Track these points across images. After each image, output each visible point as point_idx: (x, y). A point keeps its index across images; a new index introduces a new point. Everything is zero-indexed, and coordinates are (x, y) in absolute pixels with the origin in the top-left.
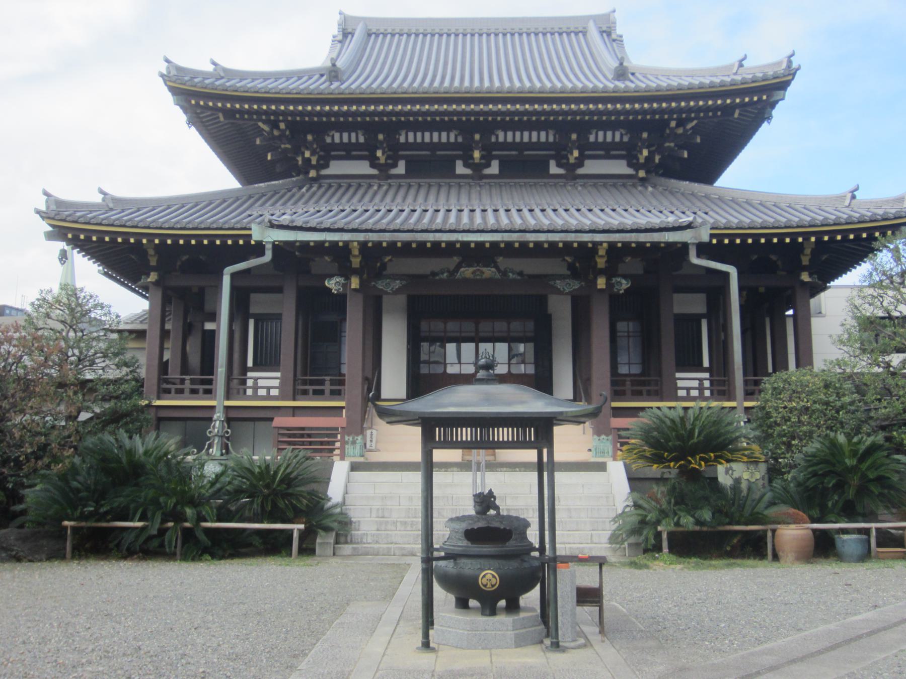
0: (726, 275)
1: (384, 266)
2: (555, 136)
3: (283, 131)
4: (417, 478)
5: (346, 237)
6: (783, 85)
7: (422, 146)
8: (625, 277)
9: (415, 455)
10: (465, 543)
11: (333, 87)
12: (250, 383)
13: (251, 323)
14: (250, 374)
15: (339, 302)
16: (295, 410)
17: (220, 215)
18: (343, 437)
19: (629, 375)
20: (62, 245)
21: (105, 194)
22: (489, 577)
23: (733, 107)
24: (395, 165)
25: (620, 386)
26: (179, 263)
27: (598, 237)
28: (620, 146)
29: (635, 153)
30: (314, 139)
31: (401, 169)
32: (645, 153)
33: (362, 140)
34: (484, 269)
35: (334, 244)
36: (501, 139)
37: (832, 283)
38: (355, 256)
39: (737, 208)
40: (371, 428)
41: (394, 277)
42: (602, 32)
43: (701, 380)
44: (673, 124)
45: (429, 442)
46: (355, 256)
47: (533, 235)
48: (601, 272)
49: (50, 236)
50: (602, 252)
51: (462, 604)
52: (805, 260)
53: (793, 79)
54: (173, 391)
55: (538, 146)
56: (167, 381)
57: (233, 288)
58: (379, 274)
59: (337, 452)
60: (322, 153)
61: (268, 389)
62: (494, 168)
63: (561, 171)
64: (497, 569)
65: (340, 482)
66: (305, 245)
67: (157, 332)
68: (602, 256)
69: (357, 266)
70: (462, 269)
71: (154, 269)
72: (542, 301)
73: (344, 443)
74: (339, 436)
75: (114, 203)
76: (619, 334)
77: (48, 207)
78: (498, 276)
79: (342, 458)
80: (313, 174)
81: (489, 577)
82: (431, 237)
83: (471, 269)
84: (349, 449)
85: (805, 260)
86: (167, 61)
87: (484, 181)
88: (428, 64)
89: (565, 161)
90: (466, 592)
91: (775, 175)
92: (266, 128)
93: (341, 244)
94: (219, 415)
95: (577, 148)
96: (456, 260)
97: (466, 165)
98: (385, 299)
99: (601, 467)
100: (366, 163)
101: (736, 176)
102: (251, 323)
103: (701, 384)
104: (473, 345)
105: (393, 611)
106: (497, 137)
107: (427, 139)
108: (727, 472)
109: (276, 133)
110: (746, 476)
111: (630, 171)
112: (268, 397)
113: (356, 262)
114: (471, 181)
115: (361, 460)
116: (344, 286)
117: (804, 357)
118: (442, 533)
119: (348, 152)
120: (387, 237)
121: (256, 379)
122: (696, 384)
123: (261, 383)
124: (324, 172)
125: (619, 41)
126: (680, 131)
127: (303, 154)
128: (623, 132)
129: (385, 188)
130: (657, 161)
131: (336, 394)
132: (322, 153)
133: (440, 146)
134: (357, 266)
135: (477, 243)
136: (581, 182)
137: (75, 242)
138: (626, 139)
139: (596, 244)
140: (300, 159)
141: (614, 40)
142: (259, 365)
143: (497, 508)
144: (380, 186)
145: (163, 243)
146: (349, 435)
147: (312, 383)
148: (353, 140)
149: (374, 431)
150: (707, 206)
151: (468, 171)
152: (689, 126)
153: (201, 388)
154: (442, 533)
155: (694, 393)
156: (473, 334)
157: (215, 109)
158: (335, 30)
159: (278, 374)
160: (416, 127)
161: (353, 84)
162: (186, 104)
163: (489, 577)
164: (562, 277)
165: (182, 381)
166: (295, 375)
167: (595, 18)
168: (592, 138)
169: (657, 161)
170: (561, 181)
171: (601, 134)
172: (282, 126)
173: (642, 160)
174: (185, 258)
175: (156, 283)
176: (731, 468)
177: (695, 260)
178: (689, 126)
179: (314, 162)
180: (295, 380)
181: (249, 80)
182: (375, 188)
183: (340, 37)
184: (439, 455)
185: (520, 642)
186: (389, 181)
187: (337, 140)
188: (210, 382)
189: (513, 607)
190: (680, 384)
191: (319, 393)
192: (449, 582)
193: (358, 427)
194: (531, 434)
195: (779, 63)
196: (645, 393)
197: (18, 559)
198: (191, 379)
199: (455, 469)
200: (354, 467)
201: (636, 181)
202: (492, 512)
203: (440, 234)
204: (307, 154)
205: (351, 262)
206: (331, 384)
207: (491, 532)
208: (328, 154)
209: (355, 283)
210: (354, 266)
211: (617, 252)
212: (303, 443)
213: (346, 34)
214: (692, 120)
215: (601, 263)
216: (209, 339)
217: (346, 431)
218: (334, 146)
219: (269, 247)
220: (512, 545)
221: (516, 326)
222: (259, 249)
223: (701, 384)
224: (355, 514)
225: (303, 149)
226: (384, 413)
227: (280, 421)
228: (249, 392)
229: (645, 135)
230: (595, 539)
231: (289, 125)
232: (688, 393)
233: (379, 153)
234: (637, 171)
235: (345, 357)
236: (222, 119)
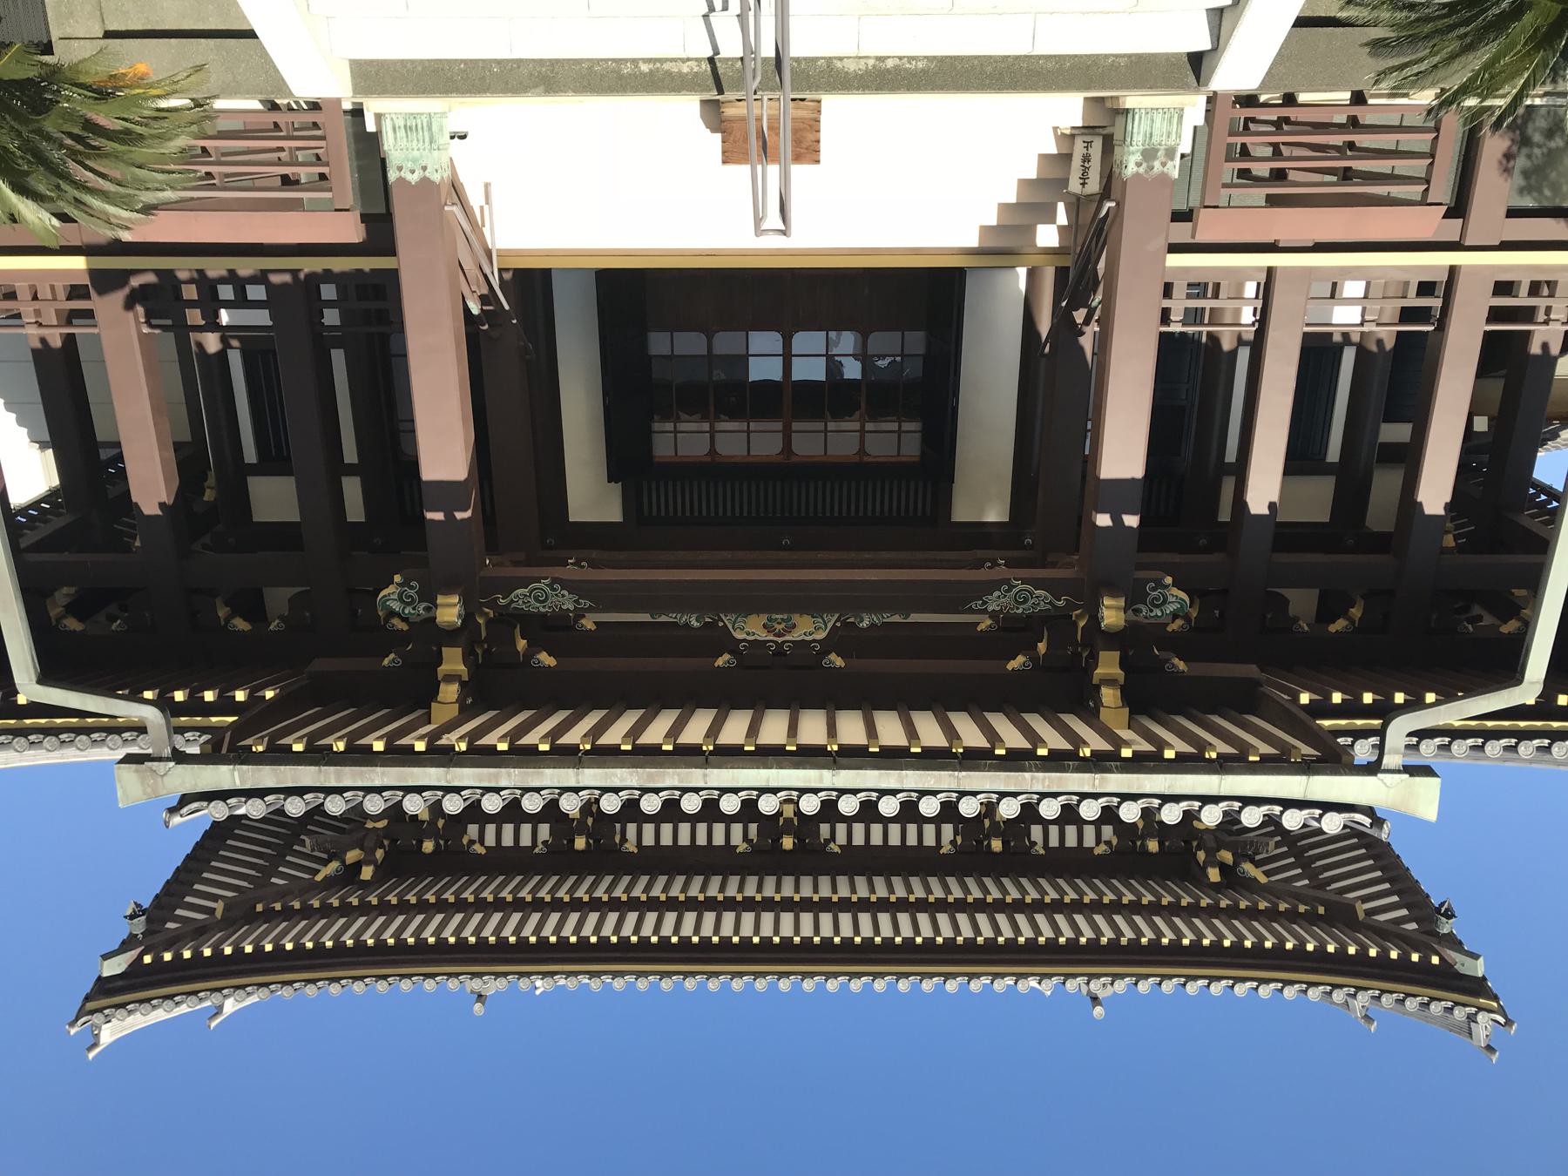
2: (624, 839)
3: (1212, 861)
13: (1334, 453)
34: (763, 635)
38: (1110, 682)
46: (1110, 682)
48: (450, 636)
50: (449, 692)
53: (87, 999)
68: (450, 678)
69: (1104, 656)
70: (821, 635)
78: (727, 620)
83: (796, 636)
91: (129, 789)
102: (1334, 453)
109: (1227, 856)
113: (1108, 665)
126: (352, 856)
128: (478, 849)
134: (1104, 656)
146: (1164, 177)
153: (1522, 300)
171: (526, 841)
172: (1214, 875)
199: (851, 66)
210: (1115, 655)
229: (428, 846)
231: (1200, 881)
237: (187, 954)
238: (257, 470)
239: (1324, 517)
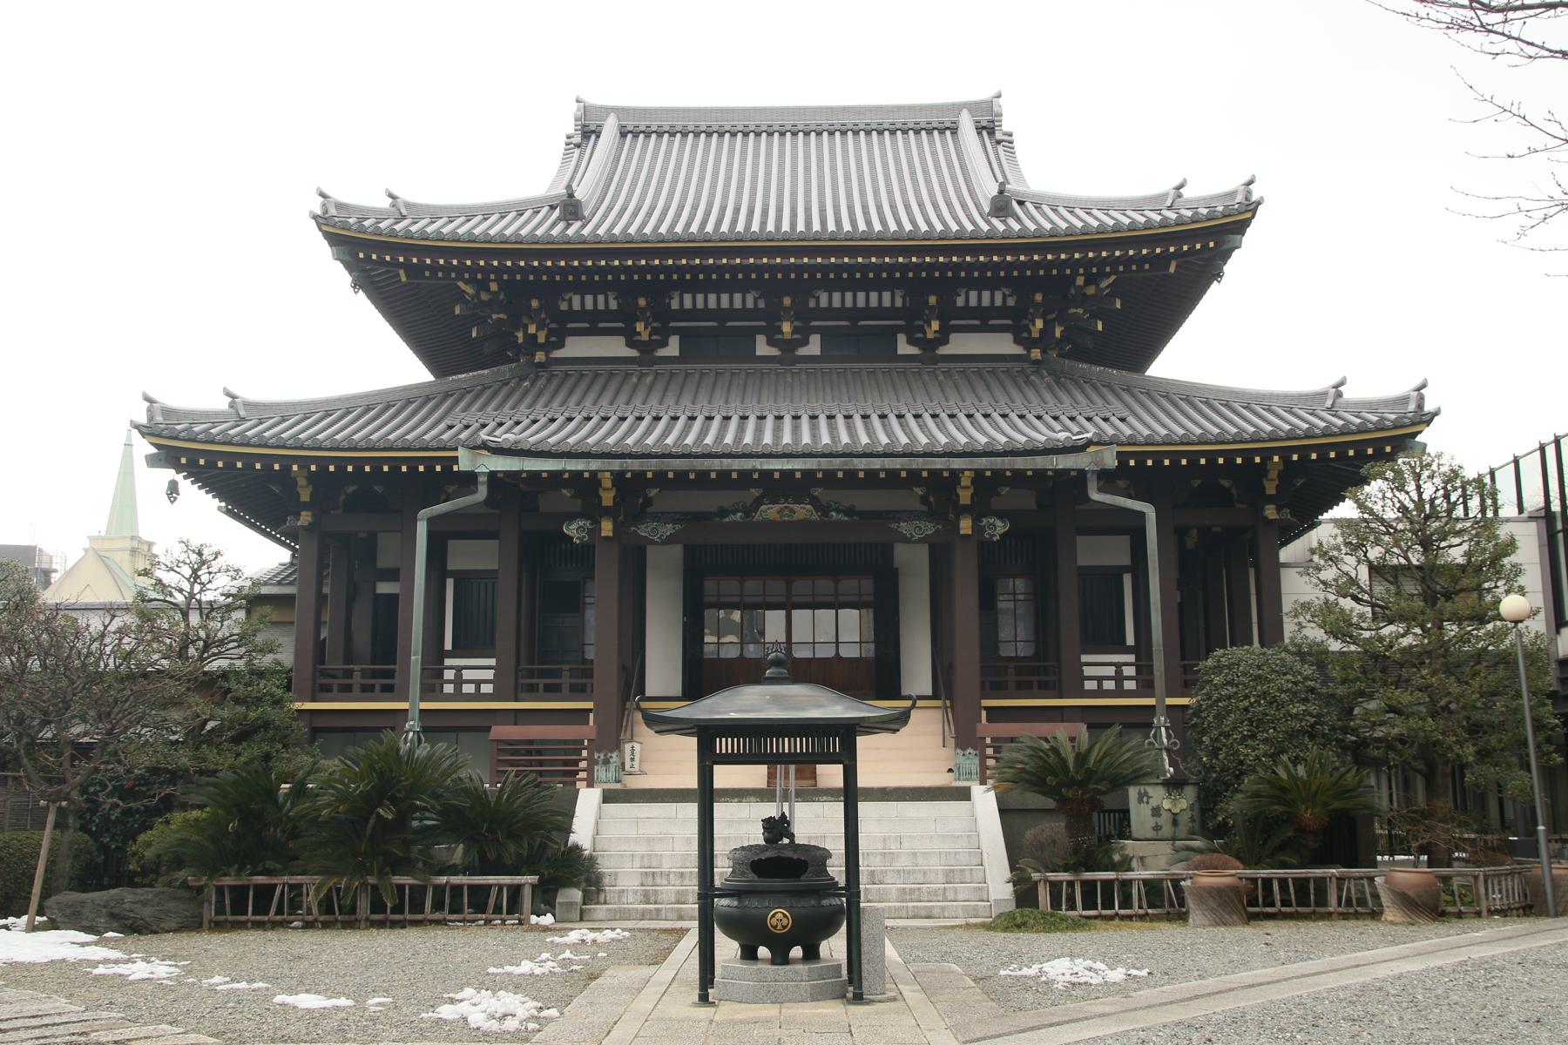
0: (1142, 515)
1: (649, 502)
4: (691, 810)
5: (594, 465)
6: (1240, 227)
7: (706, 314)
8: (1001, 515)
9: (691, 781)
10: (753, 876)
11: (570, 232)
12: (449, 675)
13: (450, 583)
14: (448, 662)
15: (585, 555)
16: (517, 716)
17: (409, 425)
18: (591, 754)
19: (1017, 659)
20: (169, 474)
21: (234, 397)
22: (779, 918)
23: (1166, 258)
25: (999, 675)
26: (343, 497)
27: (957, 463)
28: (1003, 312)
29: (1025, 322)
30: (541, 306)
31: (673, 348)
32: (1039, 324)
33: (613, 305)
34: (796, 507)
35: (577, 475)
36: (824, 303)
37: (1326, 516)
39: (1171, 409)
40: (631, 740)
41: (663, 517)
42: (980, 130)
43: (1118, 666)
44: (1080, 281)
45: (708, 759)
48: (966, 510)
49: (153, 461)
51: (749, 954)
52: (1271, 489)
54: (335, 688)
55: (880, 313)
56: (324, 674)
57: (431, 535)
58: (640, 516)
59: (582, 775)
60: (553, 326)
61: (478, 683)
62: (814, 347)
63: (913, 350)
64: (787, 908)
65: (589, 819)
66: (535, 475)
67: (312, 600)
71: (306, 506)
72: (887, 551)
73: (592, 763)
74: (585, 753)
75: (240, 409)
77: (151, 418)
78: (815, 517)
79: (590, 785)
80: (540, 357)
81: (779, 918)
82: (716, 464)
83: (777, 507)
84: (600, 771)
85: (1271, 489)
86: (322, 195)
87: (798, 366)
88: (712, 195)
89: (920, 335)
90: (751, 935)
91: (1233, 351)
92: (469, 289)
93: (586, 475)
94: (413, 724)
95: (938, 318)
96: (755, 492)
97: (771, 343)
98: (650, 549)
99: (964, 795)
100: (621, 340)
101: (1174, 362)
102: (450, 583)
103: (1119, 672)
104: (782, 613)
105: (665, 972)
106: (818, 299)
107: (712, 304)
108: (1140, 800)
109: (484, 297)
110: (1166, 805)
111: (1018, 350)
112: (478, 696)
113: (608, 498)
114: (778, 366)
115: (618, 786)
117: (1272, 633)
118: (723, 869)
119: (594, 324)
120: (654, 464)
121: (459, 669)
122: (1111, 671)
125: (1007, 142)
126: (1091, 290)
127: (526, 327)
129: (649, 379)
130: (1058, 335)
131: (579, 691)
132: (553, 326)
133: (731, 313)
135: (782, 472)
136: (944, 366)
138: (1011, 302)
139: (955, 474)
140: (520, 335)
141: (999, 142)
142: (460, 650)
143: (791, 836)
144: (642, 376)
145: (323, 469)
147: (543, 674)
148: (601, 306)
149: (637, 747)
150: (1128, 406)
151: (774, 352)
152: (1104, 284)
153: (378, 682)
154: (723, 869)
155: (1109, 685)
156: (783, 599)
157: (394, 264)
158: (570, 127)
159: (492, 662)
160: (694, 287)
161: (601, 226)
162: (348, 258)
163: (779, 916)
164: (912, 516)
165: (349, 674)
166: (518, 663)
167: (974, 107)
168: (960, 302)
169: (1058, 335)
172: (494, 287)
173: (1035, 335)
174: (351, 489)
175: (309, 528)
176: (1146, 794)
177: (1095, 496)
178: (1104, 284)
179: (541, 339)
180: (517, 671)
181: (445, 220)
182: (635, 380)
183: (577, 139)
184: (724, 776)
185: (817, 996)
186: (656, 367)
188: (390, 674)
189: (811, 954)
190: (1088, 671)
191: (553, 691)
192: (733, 927)
193: (612, 739)
194: (836, 745)
195: (1232, 194)
196: (1035, 685)
200: (608, 797)
201: (1025, 365)
204: (532, 329)
205: (600, 498)
207: (782, 865)
209: (607, 528)
210: (604, 504)
211: (987, 484)
212: (530, 763)
213: (588, 132)
214: (1108, 275)
215: (965, 497)
216: (389, 610)
217: (595, 746)
218: (572, 315)
219: (482, 479)
220: (806, 880)
221: (849, 586)
222: (470, 478)
223: (1119, 672)
224: (605, 866)
225: (525, 321)
226: (652, 721)
227: (500, 731)
228: (449, 689)
229: (1039, 297)
230: (950, 896)
232: (1100, 685)
233: (640, 327)
234: (1028, 349)
235: (591, 636)
236: (404, 279)
237: (1185, 248)
238: (1125, 569)
239: (450, 542)
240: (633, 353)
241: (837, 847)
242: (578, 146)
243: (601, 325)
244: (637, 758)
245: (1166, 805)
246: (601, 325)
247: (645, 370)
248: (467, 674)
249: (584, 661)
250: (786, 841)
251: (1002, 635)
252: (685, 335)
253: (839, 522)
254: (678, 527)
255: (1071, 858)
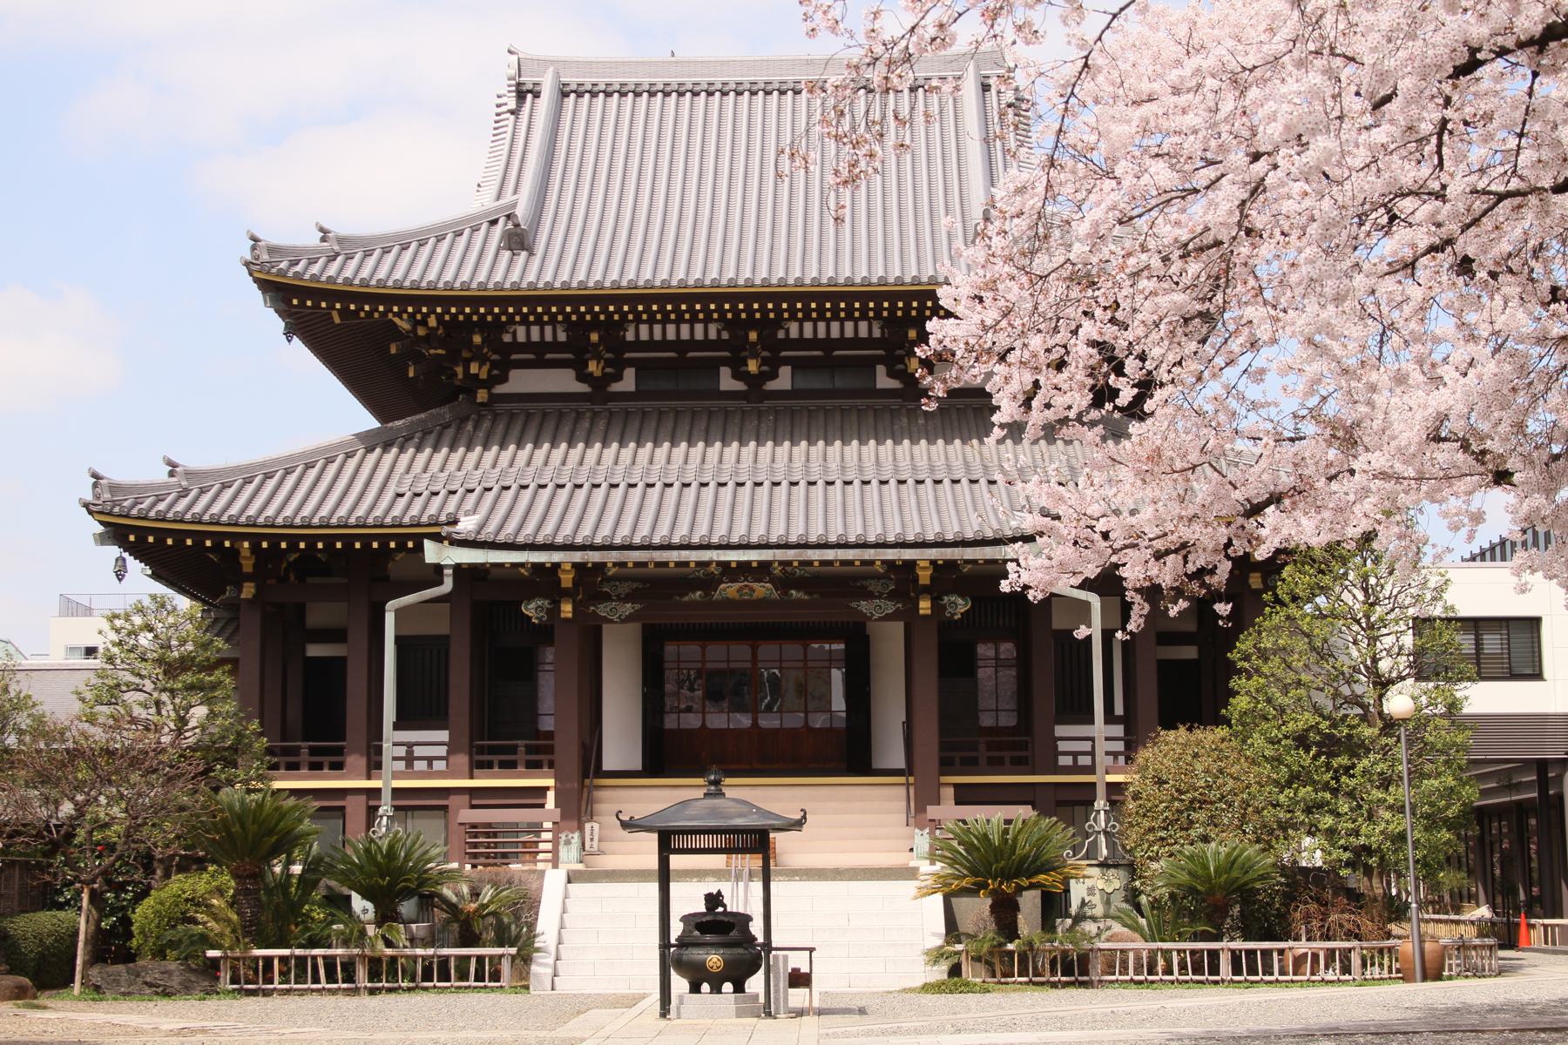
2: (882, 328)
4: (653, 888)
5: (556, 557)
9: (653, 862)
15: (546, 633)
20: (115, 551)
24: (618, 377)
34: (755, 585)
40: (591, 820)
47: (818, 552)
49: (102, 539)
51: (695, 989)
64: (719, 952)
75: (190, 480)
76: (980, 663)
78: (776, 595)
83: (737, 586)
87: (767, 403)
90: (698, 978)
98: (605, 627)
100: (570, 374)
106: (787, 331)
109: (421, 332)
115: (580, 867)
116: (549, 612)
123: (418, 751)
124: (500, 389)
131: (534, 765)
137: (140, 551)
143: (724, 906)
151: (739, 386)
154: (676, 929)
158: (505, 87)
159: (444, 735)
162: (283, 306)
170: (894, 403)
184: (676, 861)
186: (610, 405)
187: (521, 338)
189: (739, 988)
190: (1063, 746)
191: (508, 765)
192: (685, 968)
197: (167, 994)
198: (310, 748)
202: (720, 909)
203: (687, 552)
206: (527, 753)
208: (506, 360)
209: (567, 609)
218: (516, 346)
219: (449, 572)
222: (438, 569)
232: (1075, 760)
240: (583, 388)
241: (756, 911)
242: (512, 112)
243: (549, 356)
244: (596, 838)
245: (1100, 884)
246: (549, 356)
247: (597, 408)
248: (418, 751)
249: (538, 734)
250: (720, 909)
251: (982, 705)
252: (642, 368)
253: (799, 601)
254: (637, 606)
255: (1008, 925)
